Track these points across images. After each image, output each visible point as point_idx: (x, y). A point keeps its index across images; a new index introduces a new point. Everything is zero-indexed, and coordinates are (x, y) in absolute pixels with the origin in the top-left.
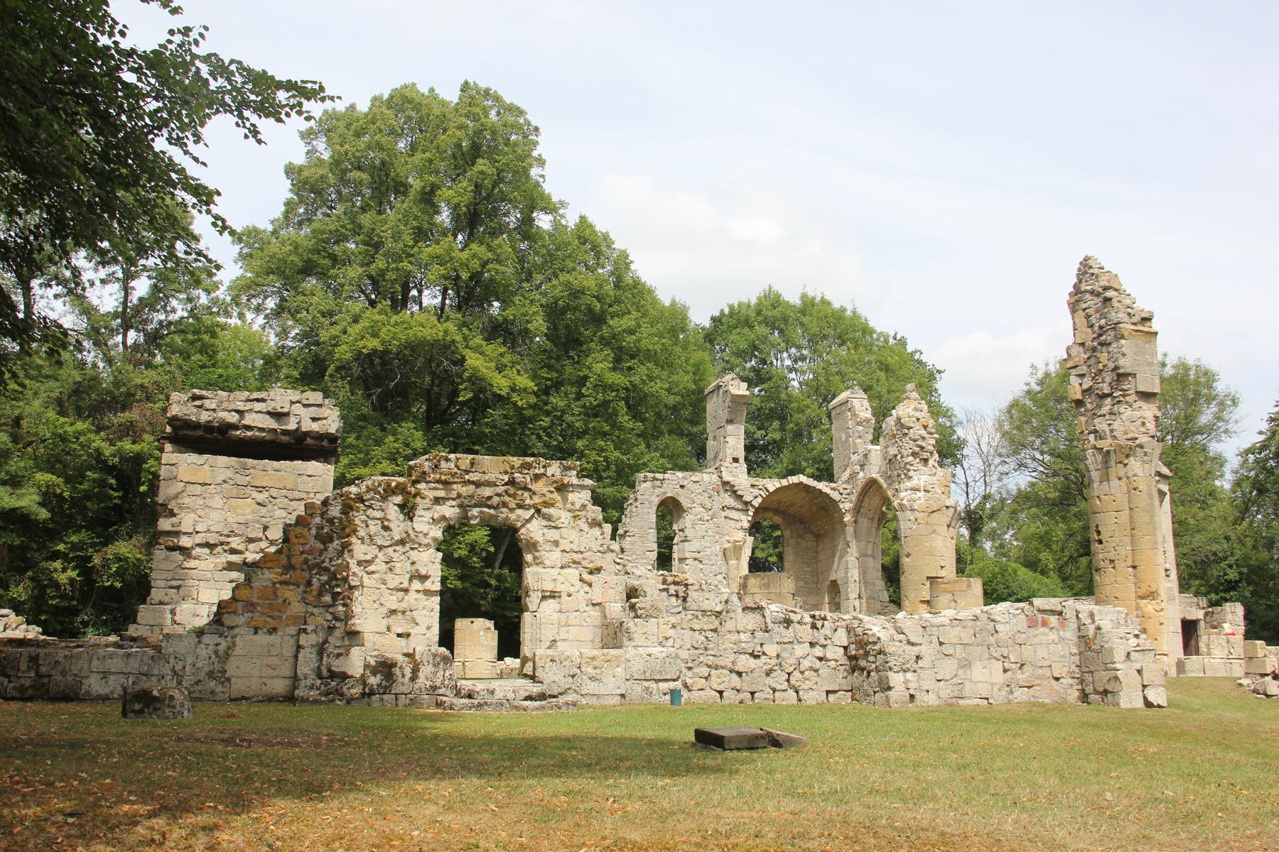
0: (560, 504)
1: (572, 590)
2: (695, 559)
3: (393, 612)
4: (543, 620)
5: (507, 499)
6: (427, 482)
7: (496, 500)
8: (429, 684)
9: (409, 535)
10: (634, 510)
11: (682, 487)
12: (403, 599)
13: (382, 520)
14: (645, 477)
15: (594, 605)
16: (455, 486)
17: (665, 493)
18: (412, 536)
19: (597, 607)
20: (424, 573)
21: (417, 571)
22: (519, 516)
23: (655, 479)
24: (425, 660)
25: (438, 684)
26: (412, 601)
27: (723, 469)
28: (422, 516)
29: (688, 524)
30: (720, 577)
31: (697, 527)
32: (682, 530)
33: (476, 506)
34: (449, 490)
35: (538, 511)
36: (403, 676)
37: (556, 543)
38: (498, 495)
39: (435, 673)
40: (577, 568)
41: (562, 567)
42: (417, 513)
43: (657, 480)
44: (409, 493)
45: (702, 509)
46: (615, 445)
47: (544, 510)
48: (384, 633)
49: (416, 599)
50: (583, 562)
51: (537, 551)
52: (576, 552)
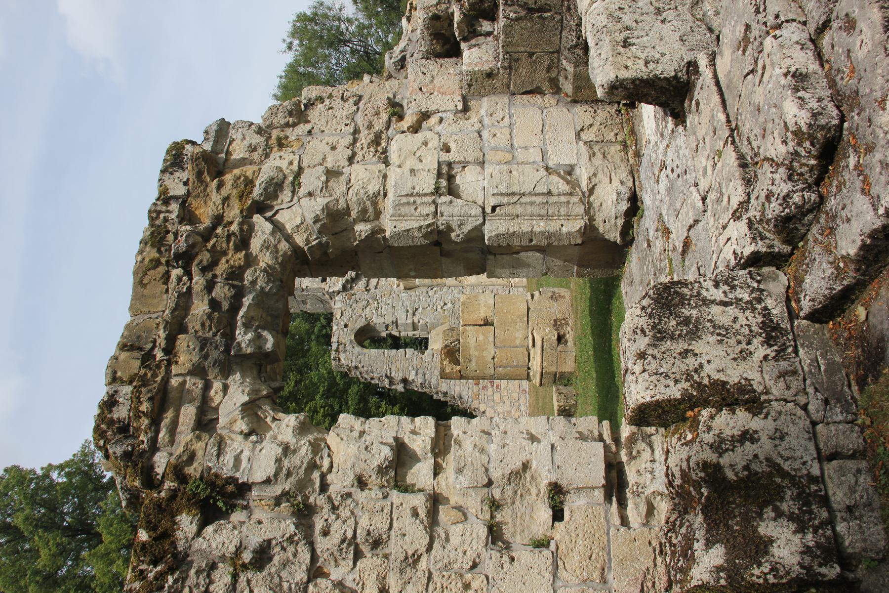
0: (249, 170)
1: (434, 143)
2: (414, 314)
3: (495, 534)
4: (503, 188)
5: (221, 268)
6: (154, 447)
7: (221, 291)
8: (760, 351)
9: (285, 495)
10: (366, 369)
11: (346, 326)
12: (459, 508)
13: (238, 568)
14: (334, 359)
15: (466, 109)
16: (174, 382)
17: (351, 341)
18: (288, 485)
19: (472, 104)
20: (386, 452)
21: (381, 471)
22: (266, 246)
23: (337, 350)
24: (680, 366)
25: (756, 320)
26: (464, 481)
27: (331, 290)
28: (237, 459)
29: (381, 320)
30: (431, 293)
31: (384, 313)
32: (387, 326)
33: (230, 336)
34: (183, 393)
35: (260, 207)
36: (746, 436)
37: (332, 174)
38: (210, 287)
39: (723, 333)
40: (389, 139)
41: (387, 163)
42: (227, 471)
43: (338, 348)
44: (173, 495)
45: (368, 309)
46: (311, 401)
47: (257, 192)
48: (555, 556)
49: (459, 471)
50: (377, 128)
51: (347, 210)
52: (355, 141)
